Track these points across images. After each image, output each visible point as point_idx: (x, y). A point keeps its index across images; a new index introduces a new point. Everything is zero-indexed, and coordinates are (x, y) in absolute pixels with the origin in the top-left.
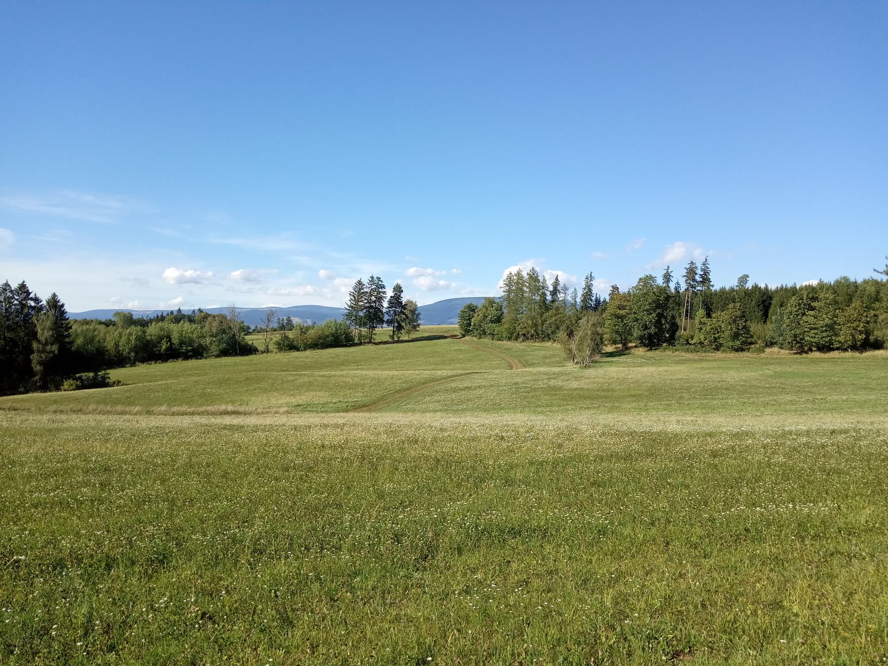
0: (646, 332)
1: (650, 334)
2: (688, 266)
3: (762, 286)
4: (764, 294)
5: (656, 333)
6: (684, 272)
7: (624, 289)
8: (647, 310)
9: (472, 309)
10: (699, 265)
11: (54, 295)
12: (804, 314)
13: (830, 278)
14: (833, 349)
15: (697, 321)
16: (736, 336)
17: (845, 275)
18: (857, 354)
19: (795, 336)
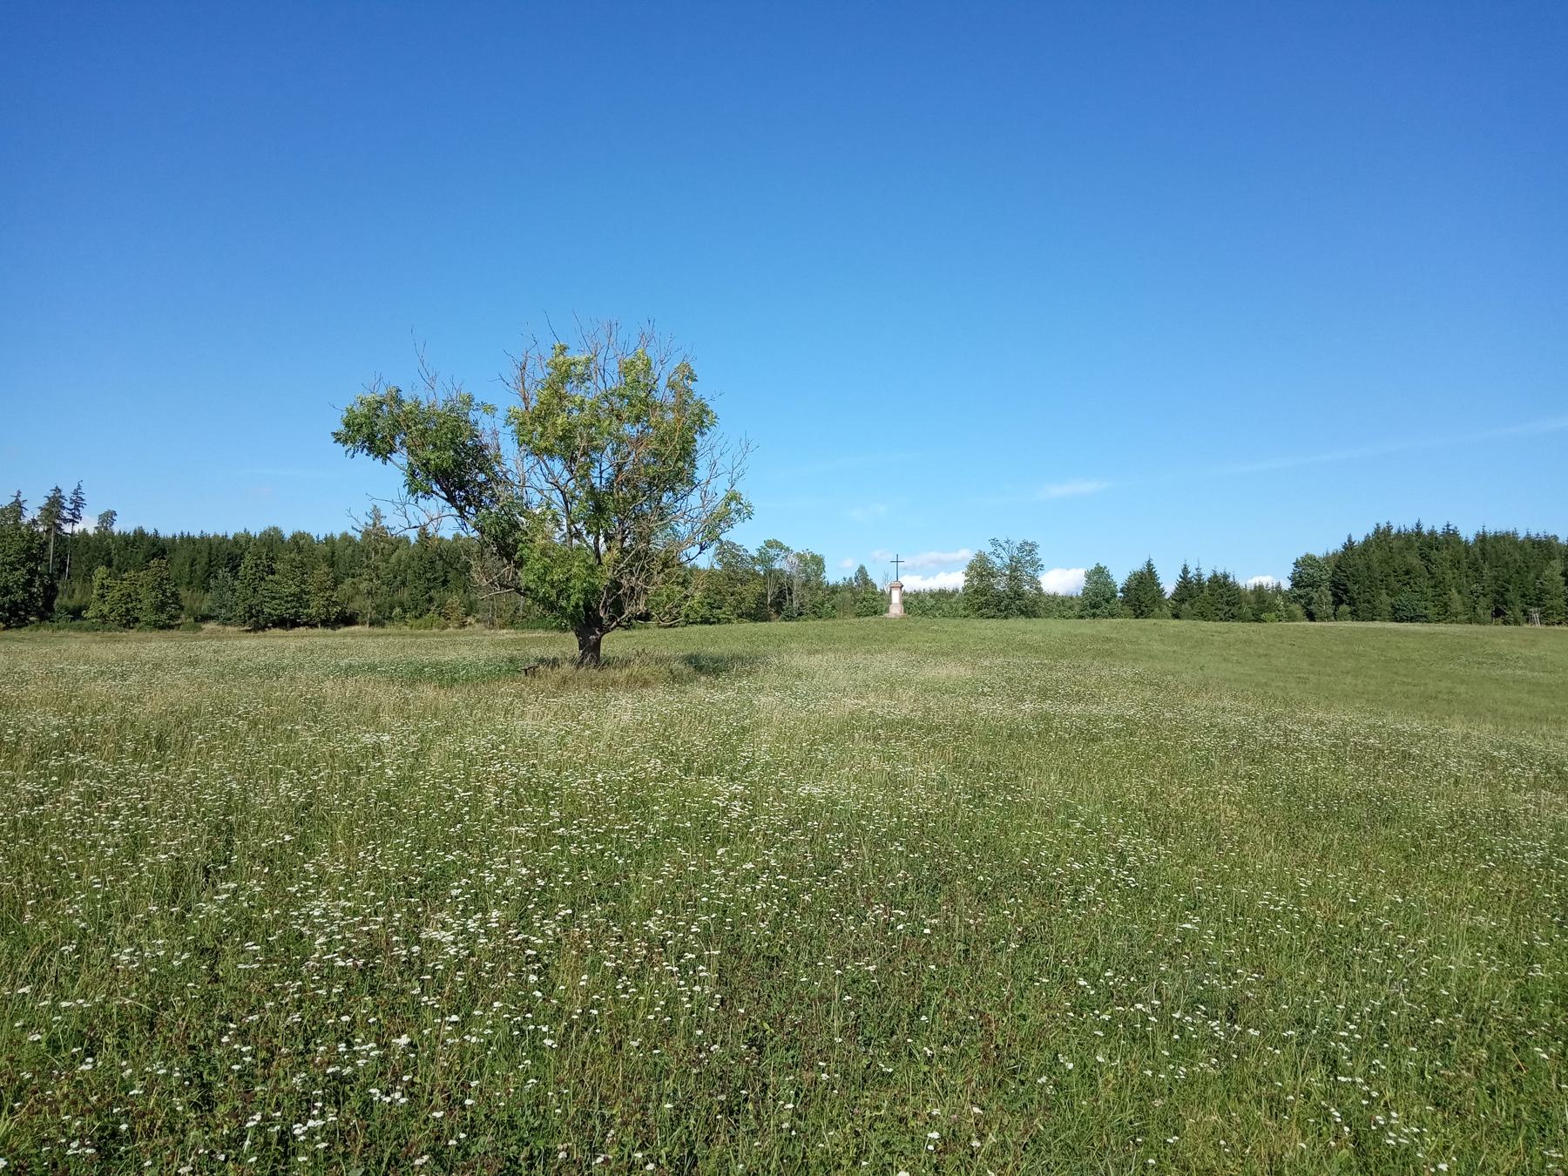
0: (6, 599)
1: (15, 603)
2: (51, 494)
3: (149, 531)
4: (154, 545)
5: (23, 601)
6: (43, 502)
7: (162, 534)
8: (11, 564)
9: (42, 617)
10: (67, 493)
11: (862, 570)
12: (263, 579)
13: (256, 530)
14: (298, 625)
15: (96, 583)
16: (161, 607)
17: (1300, 554)
18: (329, 631)
19: (251, 607)
